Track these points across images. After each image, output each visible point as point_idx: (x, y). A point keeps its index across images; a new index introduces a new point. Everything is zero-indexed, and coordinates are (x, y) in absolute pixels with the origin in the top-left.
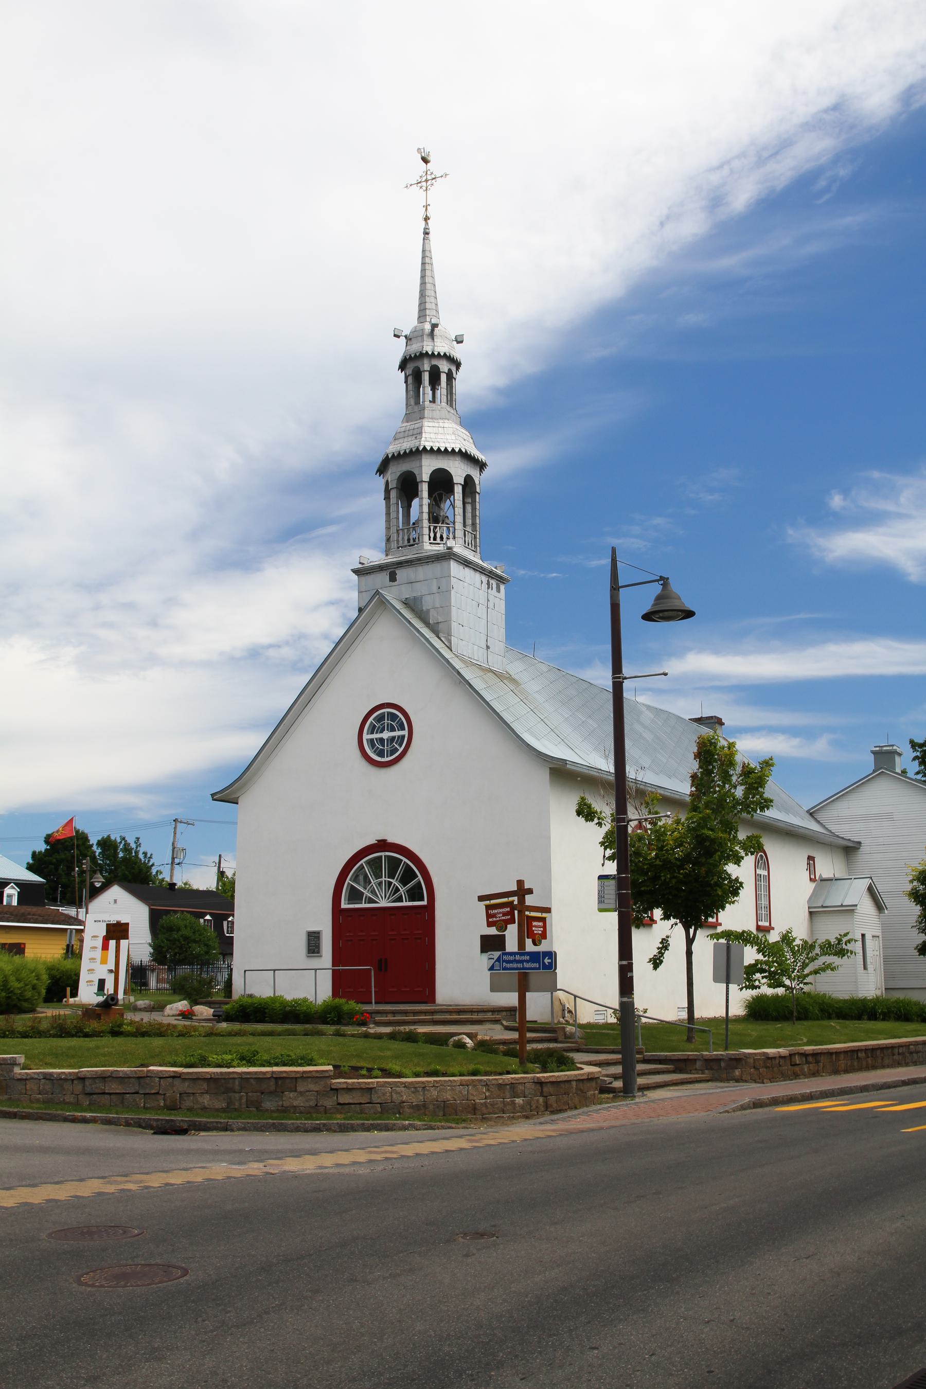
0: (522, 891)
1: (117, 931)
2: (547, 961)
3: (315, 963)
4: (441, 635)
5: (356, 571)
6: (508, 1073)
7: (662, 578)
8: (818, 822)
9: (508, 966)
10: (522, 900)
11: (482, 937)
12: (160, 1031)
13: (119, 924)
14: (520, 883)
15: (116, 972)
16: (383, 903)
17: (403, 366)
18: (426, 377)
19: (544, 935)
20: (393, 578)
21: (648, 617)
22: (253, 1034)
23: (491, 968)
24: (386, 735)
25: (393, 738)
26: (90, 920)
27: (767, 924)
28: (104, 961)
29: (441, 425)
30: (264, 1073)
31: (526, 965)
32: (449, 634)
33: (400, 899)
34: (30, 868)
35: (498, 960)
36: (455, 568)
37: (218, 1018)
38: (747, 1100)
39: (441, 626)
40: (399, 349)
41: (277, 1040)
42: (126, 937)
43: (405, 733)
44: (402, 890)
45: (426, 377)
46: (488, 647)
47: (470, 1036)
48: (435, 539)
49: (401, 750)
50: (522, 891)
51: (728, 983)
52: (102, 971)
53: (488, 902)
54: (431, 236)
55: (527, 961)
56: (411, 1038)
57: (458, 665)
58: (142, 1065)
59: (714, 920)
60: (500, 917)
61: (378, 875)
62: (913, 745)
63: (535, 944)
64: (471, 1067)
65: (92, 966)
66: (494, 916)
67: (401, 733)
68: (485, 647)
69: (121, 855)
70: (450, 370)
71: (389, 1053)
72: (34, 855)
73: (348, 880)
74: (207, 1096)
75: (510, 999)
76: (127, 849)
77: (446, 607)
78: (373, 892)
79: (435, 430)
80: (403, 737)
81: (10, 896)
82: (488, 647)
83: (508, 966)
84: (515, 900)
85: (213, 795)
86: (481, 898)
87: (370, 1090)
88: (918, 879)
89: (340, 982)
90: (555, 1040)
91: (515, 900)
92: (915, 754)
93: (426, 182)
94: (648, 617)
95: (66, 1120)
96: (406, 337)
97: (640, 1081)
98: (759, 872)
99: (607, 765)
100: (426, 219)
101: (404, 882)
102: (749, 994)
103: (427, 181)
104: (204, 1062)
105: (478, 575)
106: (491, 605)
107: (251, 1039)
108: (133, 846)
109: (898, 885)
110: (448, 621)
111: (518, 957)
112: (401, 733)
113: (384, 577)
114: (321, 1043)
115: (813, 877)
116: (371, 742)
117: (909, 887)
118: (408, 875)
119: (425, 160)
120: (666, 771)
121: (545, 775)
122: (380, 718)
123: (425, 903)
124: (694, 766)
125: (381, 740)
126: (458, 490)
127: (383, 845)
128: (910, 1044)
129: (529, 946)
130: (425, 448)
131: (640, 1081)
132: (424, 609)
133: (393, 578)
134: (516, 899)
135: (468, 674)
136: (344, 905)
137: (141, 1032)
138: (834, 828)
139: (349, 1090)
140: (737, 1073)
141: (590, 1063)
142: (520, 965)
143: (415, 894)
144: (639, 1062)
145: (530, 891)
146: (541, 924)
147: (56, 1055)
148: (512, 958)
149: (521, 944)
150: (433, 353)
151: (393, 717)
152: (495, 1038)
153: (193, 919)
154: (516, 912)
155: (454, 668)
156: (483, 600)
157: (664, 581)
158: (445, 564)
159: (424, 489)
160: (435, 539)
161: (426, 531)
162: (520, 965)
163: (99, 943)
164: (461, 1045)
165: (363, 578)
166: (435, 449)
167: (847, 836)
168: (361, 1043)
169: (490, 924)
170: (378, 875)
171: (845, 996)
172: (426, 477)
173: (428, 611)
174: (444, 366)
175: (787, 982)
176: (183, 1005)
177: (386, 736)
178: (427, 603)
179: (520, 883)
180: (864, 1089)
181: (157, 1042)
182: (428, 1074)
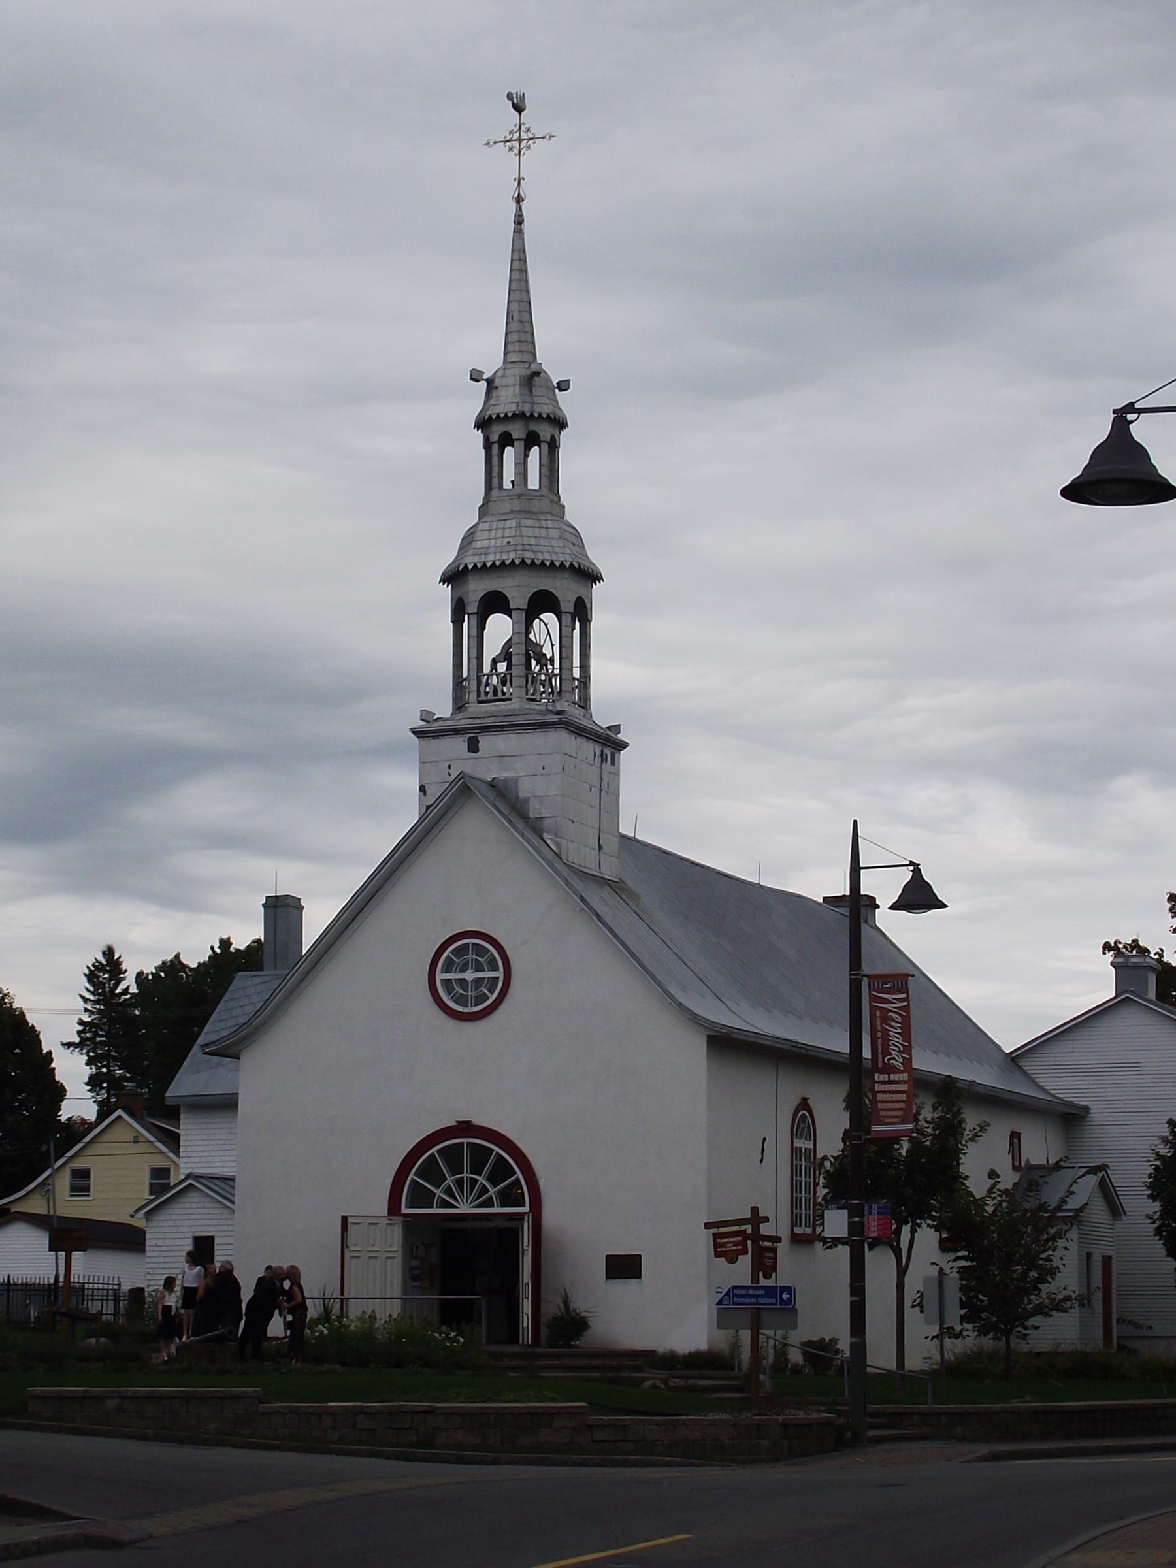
4: (545, 836)
5: (418, 733)
7: (912, 863)
9: (740, 1300)
10: (756, 1229)
11: (640, 1256)
14: (755, 1210)
16: (464, 1208)
19: (774, 1268)
20: (473, 746)
24: (469, 976)
25: (478, 982)
29: (544, 523)
31: (761, 1300)
33: (489, 1203)
39: (546, 822)
40: (474, 402)
43: (500, 974)
46: (600, 847)
53: (715, 1230)
54: (526, 226)
66: (724, 1245)
68: (597, 847)
70: (553, 438)
79: (537, 532)
82: (600, 847)
83: (740, 1300)
87: (623, 1427)
91: (749, 1229)
93: (519, 141)
96: (490, 382)
98: (797, 1143)
100: (519, 200)
101: (494, 1179)
103: (520, 140)
105: (591, 744)
109: (1133, 1173)
111: (751, 1292)
113: (460, 744)
115: (1017, 1163)
116: (447, 983)
118: (501, 1171)
119: (519, 108)
121: (698, 1046)
122: (460, 952)
127: (465, 1128)
129: (763, 1282)
132: (521, 795)
133: (473, 746)
136: (404, 1210)
139: (604, 1426)
143: (510, 1197)
145: (766, 1219)
146: (771, 1255)
148: (744, 1292)
150: (532, 415)
154: (749, 1242)
156: (596, 782)
165: (425, 742)
166: (538, 562)
167: (1068, 1097)
170: (456, 1168)
171: (687, 1352)
174: (545, 432)
177: (470, 979)
179: (755, 1210)
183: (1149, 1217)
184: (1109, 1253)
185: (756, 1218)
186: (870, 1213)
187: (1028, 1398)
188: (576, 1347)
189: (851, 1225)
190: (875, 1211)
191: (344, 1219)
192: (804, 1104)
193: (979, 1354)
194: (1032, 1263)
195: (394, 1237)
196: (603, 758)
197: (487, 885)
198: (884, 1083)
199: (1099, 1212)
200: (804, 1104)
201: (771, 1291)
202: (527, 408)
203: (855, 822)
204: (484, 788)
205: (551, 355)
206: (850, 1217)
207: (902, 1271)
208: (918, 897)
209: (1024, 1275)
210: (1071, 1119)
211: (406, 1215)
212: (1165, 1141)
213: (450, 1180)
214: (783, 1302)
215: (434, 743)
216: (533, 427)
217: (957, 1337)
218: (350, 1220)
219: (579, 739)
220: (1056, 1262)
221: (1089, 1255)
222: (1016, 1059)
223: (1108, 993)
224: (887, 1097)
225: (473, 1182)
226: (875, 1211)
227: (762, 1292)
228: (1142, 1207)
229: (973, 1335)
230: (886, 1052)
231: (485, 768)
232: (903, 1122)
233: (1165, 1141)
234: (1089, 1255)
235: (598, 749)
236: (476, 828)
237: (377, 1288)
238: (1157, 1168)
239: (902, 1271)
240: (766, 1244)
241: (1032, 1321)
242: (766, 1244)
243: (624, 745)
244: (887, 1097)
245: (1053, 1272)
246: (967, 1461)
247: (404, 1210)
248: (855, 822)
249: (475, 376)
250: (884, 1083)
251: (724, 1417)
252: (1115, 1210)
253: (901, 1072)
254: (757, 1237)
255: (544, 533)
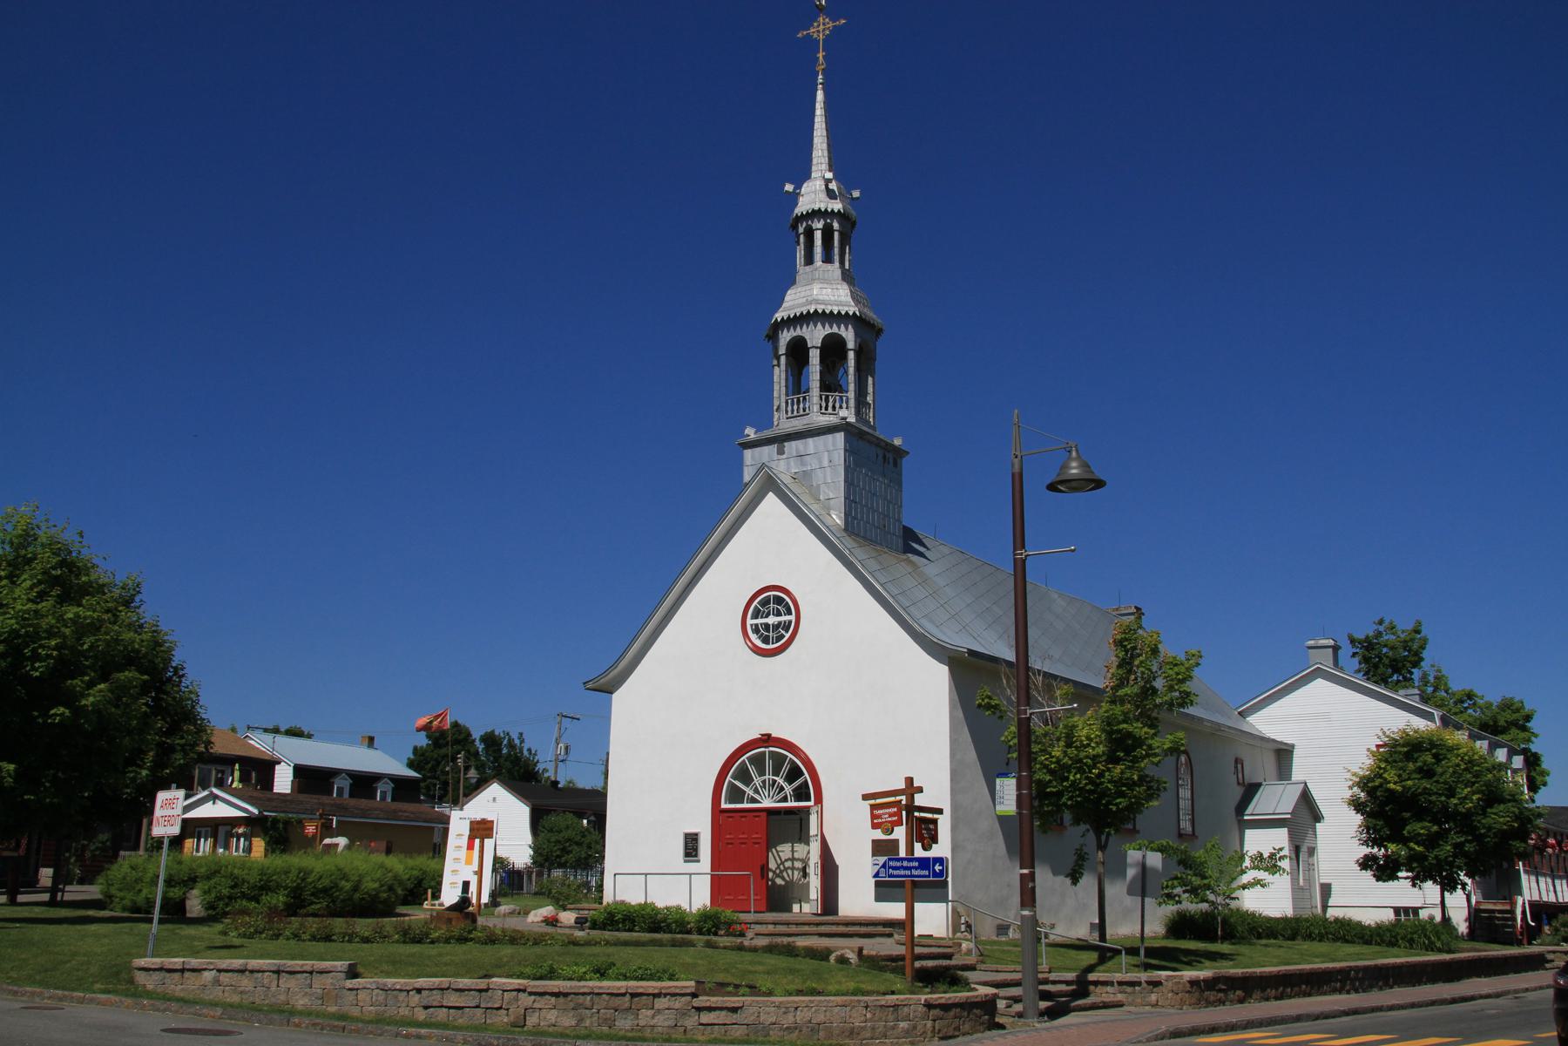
1: (482, 830)
2: (937, 868)
3: (692, 867)
6: (893, 993)
12: (515, 938)
13: (484, 821)
14: (909, 781)
15: (480, 873)
16: (767, 803)
22: (608, 943)
23: (876, 875)
24: (772, 620)
25: (777, 626)
26: (455, 815)
28: (469, 862)
31: (915, 872)
33: (785, 799)
34: (411, 765)
35: (884, 866)
37: (580, 922)
41: (639, 950)
42: (490, 836)
43: (792, 618)
44: (788, 789)
49: (787, 636)
51: (1143, 895)
52: (468, 873)
56: (790, 951)
58: (485, 976)
59: (1130, 826)
60: (886, 818)
61: (762, 773)
62: (1353, 641)
63: (925, 848)
64: (852, 985)
65: (457, 866)
66: (879, 817)
67: (788, 618)
69: (505, 751)
71: (760, 968)
72: (415, 749)
74: (555, 1012)
75: (896, 910)
76: (511, 745)
86: (866, 797)
88: (1358, 784)
89: (718, 886)
94: (1052, 487)
99: (1010, 656)
102: (1170, 909)
104: (551, 974)
107: (611, 950)
108: (517, 742)
111: (905, 864)
112: (788, 618)
114: (687, 955)
117: (1348, 794)
118: (794, 774)
120: (1075, 653)
122: (765, 602)
124: (1112, 657)
125: (767, 626)
127: (767, 740)
128: (1351, 968)
129: (919, 852)
136: (724, 806)
137: (491, 939)
140: (1153, 997)
141: (985, 984)
143: (801, 794)
145: (920, 790)
147: (394, 963)
149: (910, 849)
151: (779, 601)
152: (206, 929)
153: (576, 820)
161: (816, 399)
163: (464, 841)
164: (842, 960)
168: (732, 956)
169: (875, 826)
170: (762, 773)
175: (1211, 897)
176: (547, 910)
179: (909, 781)
180: (1298, 1018)
181: (507, 951)
182: (800, 992)
185: (911, 788)
201: (924, 863)
214: (935, 874)
254: (911, 808)
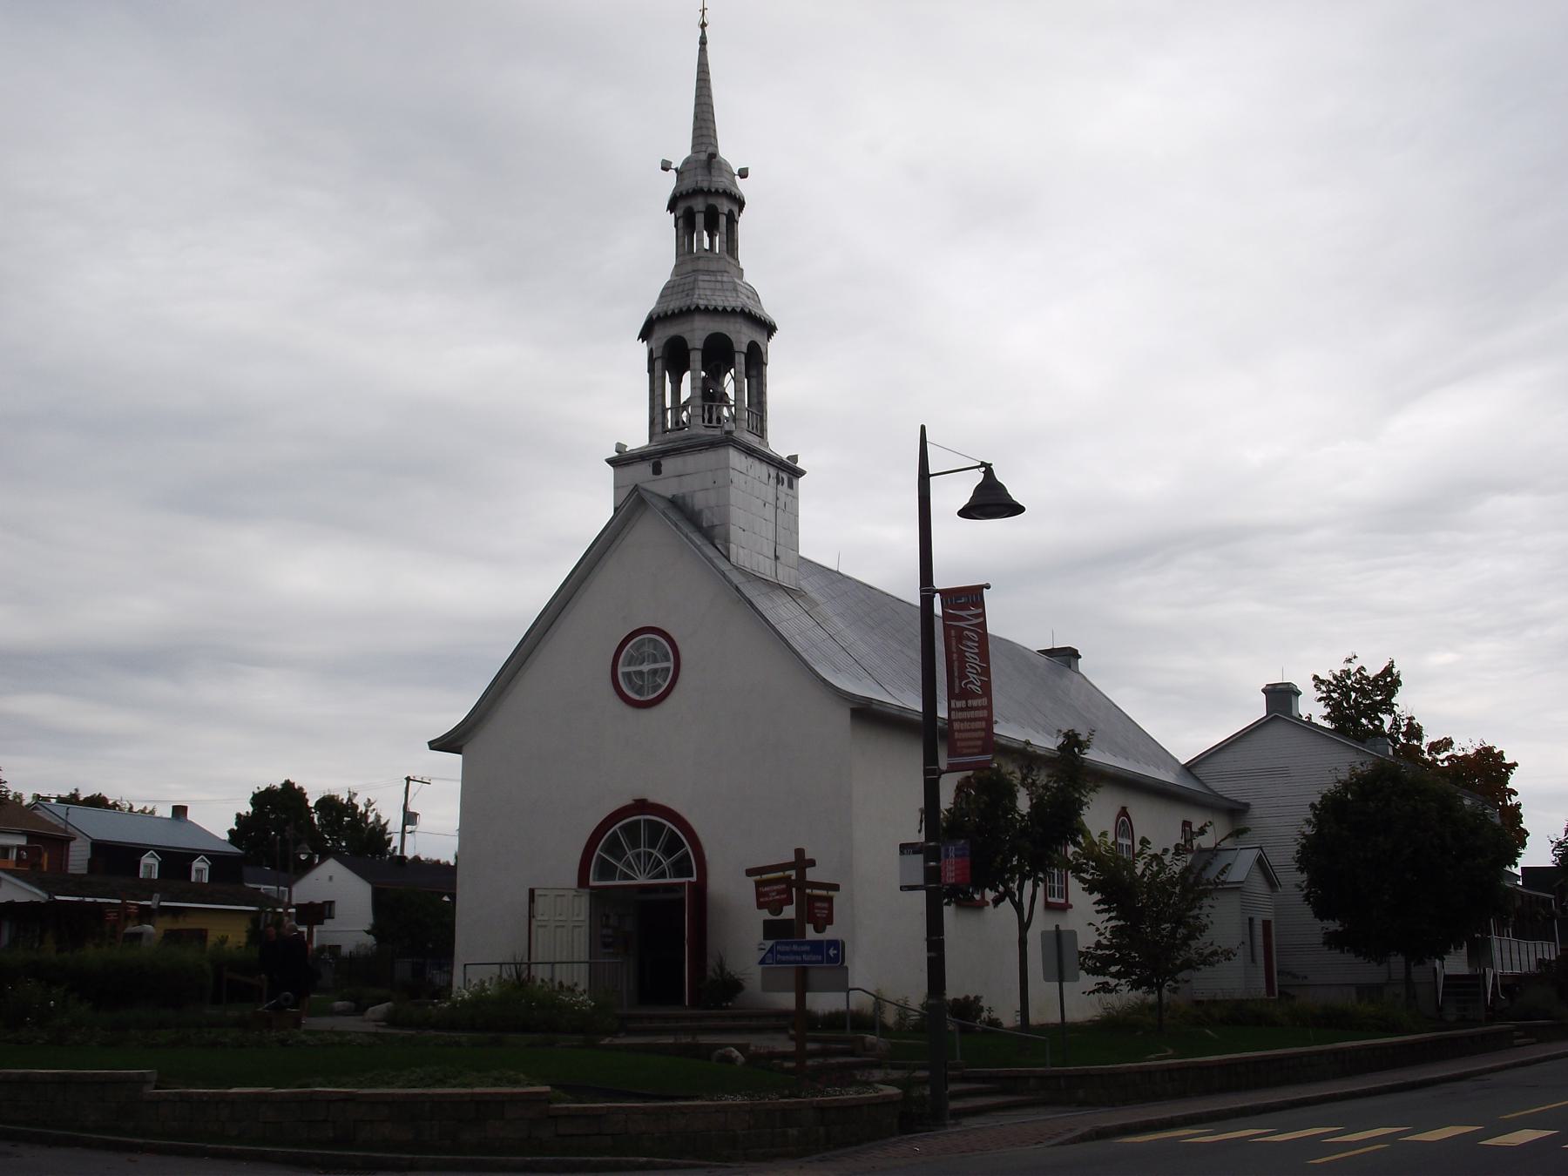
0: (802, 862)
7: (983, 465)
8: (1197, 779)
14: (799, 853)
16: (642, 880)
17: (672, 207)
18: (700, 220)
20: (657, 470)
21: (966, 513)
23: (762, 962)
24: (645, 668)
25: (654, 672)
27: (1062, 901)
30: (461, 1095)
32: (727, 541)
33: (662, 875)
35: (771, 951)
36: (736, 458)
38: (1086, 1129)
40: (669, 182)
43: (671, 665)
45: (700, 220)
46: (777, 558)
47: (737, 1047)
48: (710, 421)
50: (802, 862)
54: (709, 47)
55: (807, 953)
57: (736, 578)
60: (774, 896)
63: (817, 931)
66: (766, 894)
70: (731, 212)
73: (598, 851)
77: (724, 507)
78: (630, 866)
79: (712, 285)
80: (668, 669)
81: (199, 871)
82: (777, 558)
84: (793, 873)
85: (430, 743)
86: (750, 873)
90: (851, 1053)
92: (1320, 695)
95: (216, 1155)
97: (954, 1105)
100: (703, 25)
106: (781, 504)
109: (1284, 856)
110: (725, 525)
113: (645, 469)
116: (627, 675)
118: (673, 845)
121: (843, 716)
123: (694, 879)
125: (641, 673)
126: (740, 360)
127: (641, 806)
128: (1303, 1055)
130: (697, 307)
131: (954, 1105)
133: (657, 470)
134: (793, 873)
135: (749, 591)
136: (592, 883)
138: (1216, 786)
142: (798, 958)
143: (681, 868)
144: (954, 1080)
145: (812, 863)
146: (826, 905)
155: (730, 582)
156: (771, 499)
157: (988, 469)
158: (721, 452)
159: (696, 358)
160: (710, 421)
162: (798, 958)
164: (729, 1060)
167: (1232, 796)
170: (635, 844)
172: (699, 344)
173: (700, 512)
174: (724, 206)
178: (699, 501)
179: (799, 853)
183: (1298, 886)
184: (1268, 918)
186: (947, 856)
187: (1170, 1052)
188: (727, 1007)
189: (928, 870)
190: (952, 854)
191: (532, 892)
192: (1124, 812)
193: (1141, 1008)
194: (1179, 921)
195: (584, 902)
196: (779, 481)
197: (664, 590)
198: (961, 709)
199: (1259, 885)
200: (1124, 812)
202: (705, 185)
203: (923, 428)
204: (662, 505)
205: (730, 151)
206: (926, 861)
207: (1024, 927)
208: (991, 501)
209: (1174, 931)
210: (1235, 812)
211: (593, 888)
212: (1308, 822)
213: (630, 854)
215: (626, 469)
216: (712, 201)
217: (1110, 991)
218: (537, 892)
219: (750, 460)
220: (1205, 920)
221: (1251, 920)
222: (1190, 768)
223: (1262, 712)
224: (966, 725)
225: (638, 855)
226: (952, 854)
227: (807, 948)
228: (1293, 879)
229: (1125, 989)
230: (963, 676)
231: (666, 486)
232: (984, 752)
233: (1308, 822)
234: (1251, 920)
235: (773, 472)
236: (651, 531)
237: (565, 953)
238: (1303, 846)
239: (1024, 927)
240: (816, 892)
241: (1180, 976)
242: (816, 892)
243: (802, 473)
244: (966, 725)
245: (1202, 929)
246: (1062, 1144)
247: (592, 883)
248: (923, 428)
249: (666, 167)
250: (961, 709)
251: (739, 1100)
252: (1272, 883)
253: (980, 697)
254: (802, 884)
255: (719, 286)
